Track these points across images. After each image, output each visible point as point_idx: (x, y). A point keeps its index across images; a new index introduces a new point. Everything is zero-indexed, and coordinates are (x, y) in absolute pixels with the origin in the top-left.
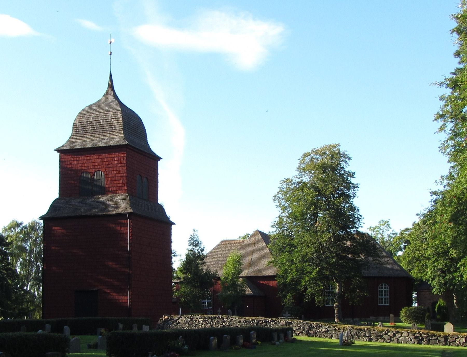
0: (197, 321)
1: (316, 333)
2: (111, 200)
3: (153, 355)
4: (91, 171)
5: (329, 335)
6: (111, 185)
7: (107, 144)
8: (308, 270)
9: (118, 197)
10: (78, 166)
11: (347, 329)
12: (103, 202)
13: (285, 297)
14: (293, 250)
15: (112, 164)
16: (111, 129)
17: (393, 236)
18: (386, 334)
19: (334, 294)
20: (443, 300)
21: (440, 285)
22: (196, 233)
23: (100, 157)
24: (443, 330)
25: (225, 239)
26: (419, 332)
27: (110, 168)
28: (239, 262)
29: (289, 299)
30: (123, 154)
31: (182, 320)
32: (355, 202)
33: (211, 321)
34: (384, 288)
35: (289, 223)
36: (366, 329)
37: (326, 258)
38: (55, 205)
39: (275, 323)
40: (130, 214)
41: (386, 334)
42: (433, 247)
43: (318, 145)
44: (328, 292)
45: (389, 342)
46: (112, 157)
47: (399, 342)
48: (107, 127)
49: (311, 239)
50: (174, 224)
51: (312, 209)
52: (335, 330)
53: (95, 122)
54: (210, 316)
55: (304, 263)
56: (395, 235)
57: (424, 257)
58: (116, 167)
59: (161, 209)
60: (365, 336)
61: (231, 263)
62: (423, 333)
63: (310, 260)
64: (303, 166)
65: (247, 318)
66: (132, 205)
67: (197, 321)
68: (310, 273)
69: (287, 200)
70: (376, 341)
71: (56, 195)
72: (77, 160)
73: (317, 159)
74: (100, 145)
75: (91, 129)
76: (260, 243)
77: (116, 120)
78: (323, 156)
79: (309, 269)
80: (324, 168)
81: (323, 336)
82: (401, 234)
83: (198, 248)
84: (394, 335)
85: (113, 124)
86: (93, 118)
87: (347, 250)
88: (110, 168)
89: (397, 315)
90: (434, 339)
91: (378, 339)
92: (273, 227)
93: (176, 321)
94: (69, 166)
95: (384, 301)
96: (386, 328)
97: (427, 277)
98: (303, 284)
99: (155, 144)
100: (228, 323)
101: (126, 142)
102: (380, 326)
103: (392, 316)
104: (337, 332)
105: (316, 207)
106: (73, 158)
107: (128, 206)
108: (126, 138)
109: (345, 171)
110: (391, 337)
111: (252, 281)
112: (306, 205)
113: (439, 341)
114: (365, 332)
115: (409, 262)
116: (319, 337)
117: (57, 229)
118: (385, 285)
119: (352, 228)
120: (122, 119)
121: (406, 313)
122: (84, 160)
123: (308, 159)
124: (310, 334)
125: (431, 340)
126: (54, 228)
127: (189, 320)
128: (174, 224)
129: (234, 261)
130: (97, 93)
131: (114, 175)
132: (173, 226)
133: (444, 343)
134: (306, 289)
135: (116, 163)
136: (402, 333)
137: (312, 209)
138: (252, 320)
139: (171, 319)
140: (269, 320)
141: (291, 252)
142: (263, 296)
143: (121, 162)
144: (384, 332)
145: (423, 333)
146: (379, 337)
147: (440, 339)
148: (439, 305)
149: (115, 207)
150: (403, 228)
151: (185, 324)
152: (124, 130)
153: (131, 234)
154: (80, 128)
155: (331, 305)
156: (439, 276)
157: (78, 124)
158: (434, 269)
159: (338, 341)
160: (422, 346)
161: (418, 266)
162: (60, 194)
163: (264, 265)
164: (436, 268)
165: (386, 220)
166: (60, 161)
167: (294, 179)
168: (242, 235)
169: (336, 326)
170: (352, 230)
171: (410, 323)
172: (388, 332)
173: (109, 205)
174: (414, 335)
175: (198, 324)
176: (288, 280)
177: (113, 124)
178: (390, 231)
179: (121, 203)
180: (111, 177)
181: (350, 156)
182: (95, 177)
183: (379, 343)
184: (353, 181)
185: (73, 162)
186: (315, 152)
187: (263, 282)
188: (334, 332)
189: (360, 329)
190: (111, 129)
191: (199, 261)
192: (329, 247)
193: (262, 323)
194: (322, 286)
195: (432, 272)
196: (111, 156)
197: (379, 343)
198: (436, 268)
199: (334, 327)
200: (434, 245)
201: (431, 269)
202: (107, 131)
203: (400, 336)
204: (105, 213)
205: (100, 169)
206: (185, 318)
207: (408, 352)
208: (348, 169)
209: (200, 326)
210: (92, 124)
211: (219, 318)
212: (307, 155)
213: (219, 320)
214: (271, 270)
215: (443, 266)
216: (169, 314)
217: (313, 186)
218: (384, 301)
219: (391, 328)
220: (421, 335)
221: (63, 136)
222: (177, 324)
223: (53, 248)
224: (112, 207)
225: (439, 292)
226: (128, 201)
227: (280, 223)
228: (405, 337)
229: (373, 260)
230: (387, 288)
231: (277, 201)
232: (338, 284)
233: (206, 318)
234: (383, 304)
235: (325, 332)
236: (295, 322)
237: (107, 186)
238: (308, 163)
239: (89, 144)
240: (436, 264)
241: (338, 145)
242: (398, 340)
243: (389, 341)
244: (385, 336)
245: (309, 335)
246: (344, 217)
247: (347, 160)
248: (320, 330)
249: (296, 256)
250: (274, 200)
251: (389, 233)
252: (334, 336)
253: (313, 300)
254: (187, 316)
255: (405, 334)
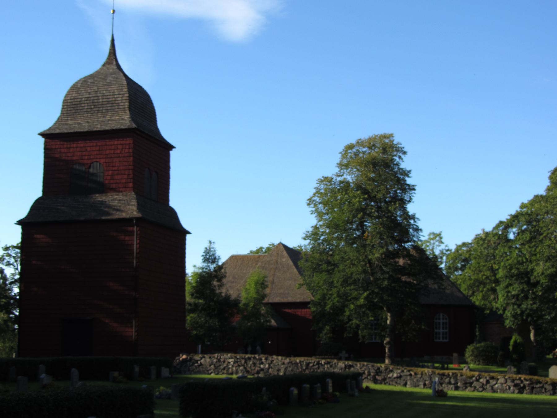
0: (226, 362)
1: (384, 379)
2: (112, 200)
3: (237, 415)
4: (86, 161)
5: (412, 382)
6: (112, 181)
7: (108, 127)
8: (353, 295)
9: (120, 196)
10: (69, 155)
11: (426, 374)
12: (102, 203)
13: (321, 329)
14: (333, 269)
15: (121, 153)
16: (113, 108)
17: (447, 253)
18: (477, 380)
19: (385, 327)
20: (519, 334)
21: (515, 316)
22: (212, 246)
23: (99, 144)
24: (547, 376)
25: (235, 253)
26: (520, 378)
27: (110, 158)
28: (263, 284)
29: (325, 334)
30: (129, 141)
31: (205, 361)
32: (411, 208)
33: (246, 362)
34: (442, 319)
35: (327, 234)
36: (451, 374)
37: (376, 280)
38: (37, 206)
39: (331, 366)
40: (138, 219)
41: (477, 380)
42: (506, 267)
43: (365, 134)
44: (378, 325)
45: (482, 391)
46: (114, 145)
47: (494, 391)
48: (108, 105)
49: (358, 255)
50: (189, 233)
51: (359, 216)
52: (411, 375)
53: (92, 98)
54: (243, 355)
55: (348, 286)
56: (449, 252)
57: (489, 279)
58: (119, 157)
59: (173, 214)
60: (450, 383)
61: (253, 285)
62: (525, 379)
63: (355, 282)
64: (345, 161)
65: (293, 359)
66: (140, 208)
67: (226, 362)
68: (356, 299)
69: (325, 203)
70: (463, 390)
71: (38, 193)
72: (67, 148)
73: (364, 153)
74: (98, 128)
75: (86, 107)
76: (284, 260)
77: (121, 96)
78: (372, 149)
79: (355, 293)
80: (374, 164)
81: (394, 383)
82: (457, 250)
83: (215, 265)
84: (488, 382)
85: (117, 102)
86: (90, 93)
87: (402, 270)
88: (110, 158)
89: (462, 354)
90: (540, 387)
91: (466, 388)
92: (305, 239)
93: (197, 362)
94: (57, 156)
95: (441, 336)
96: (476, 374)
97: (498, 305)
98: (347, 313)
99: (166, 128)
100: (267, 366)
101: (134, 126)
102: (467, 370)
103: (455, 355)
104: (413, 377)
105: (365, 214)
106: (63, 145)
107: (134, 208)
108: (133, 118)
109: (399, 169)
110: (483, 384)
111: (278, 308)
112: (352, 211)
113: (545, 389)
114: (450, 378)
115: (470, 287)
116: (389, 384)
117: (41, 238)
118: (443, 316)
119: (408, 241)
120: (127, 95)
121: (473, 351)
122: (77, 147)
123: (351, 152)
124: (377, 380)
125: (536, 388)
126: (35, 236)
127: (215, 360)
128: (189, 233)
129: (257, 283)
130: (94, 63)
131: (116, 168)
132: (188, 236)
133: (552, 392)
134: (350, 320)
135: (119, 151)
136: (498, 379)
137: (359, 216)
138: (300, 362)
139: (191, 359)
140: (323, 362)
141: (329, 272)
142: (287, 328)
143: (127, 151)
144: (474, 378)
145: (525, 379)
146: (467, 384)
147: (547, 386)
148: (515, 342)
149: (118, 210)
150: (460, 243)
151: (210, 366)
152: (130, 109)
153: (138, 245)
154: (72, 105)
155: (378, 340)
156: (514, 304)
157: (69, 101)
158: (507, 296)
159: (429, 391)
160: (525, 396)
161: (482, 291)
162: (44, 191)
163: (291, 288)
164: (509, 294)
165: (437, 232)
166: (46, 149)
167: (335, 178)
168: (254, 249)
169: (412, 370)
170: (408, 245)
171: (479, 365)
172: (480, 378)
173: (110, 207)
174: (513, 381)
175: (227, 366)
176: (328, 308)
177: (117, 102)
178: (443, 247)
179: (125, 205)
180: (112, 170)
181: (405, 150)
182: (91, 170)
183: (468, 393)
184: (409, 181)
185: (63, 150)
186: (360, 143)
187: (290, 311)
188: (408, 378)
189: (443, 375)
190: (113, 108)
191: (215, 283)
192: (381, 266)
193: (314, 365)
194: (372, 316)
195: (504, 300)
196: (112, 143)
197: (468, 393)
198: (509, 294)
199: (409, 371)
200: (507, 265)
201: (503, 296)
202: (107, 111)
203: (494, 382)
204: (103, 218)
205: (98, 160)
206: (210, 358)
207: (548, 406)
208: (403, 166)
209: (229, 368)
210: (88, 102)
211: (254, 358)
212: (350, 147)
213: (255, 361)
214: (301, 294)
215: (519, 291)
216: (188, 352)
217: (358, 187)
218: (441, 336)
219: (483, 374)
220: (522, 382)
221: (49, 116)
222: (199, 366)
223: (34, 262)
224: (114, 209)
225: (513, 324)
226: (134, 202)
227: (314, 235)
228: (502, 384)
229: (434, 284)
230: (446, 319)
231: (312, 205)
232: (389, 314)
233: (238, 359)
234: (441, 340)
235: (397, 377)
236: (356, 365)
237: (107, 182)
238: (351, 157)
239: (84, 127)
240: (510, 288)
241: (391, 135)
242: (492, 387)
243: (481, 389)
244: (475, 384)
245: (375, 381)
246: (400, 227)
247: (401, 155)
248: (390, 375)
249: (337, 278)
250: (309, 204)
251: (440, 248)
252: (409, 383)
253: (356, 334)
254: (212, 356)
255: (501, 380)
